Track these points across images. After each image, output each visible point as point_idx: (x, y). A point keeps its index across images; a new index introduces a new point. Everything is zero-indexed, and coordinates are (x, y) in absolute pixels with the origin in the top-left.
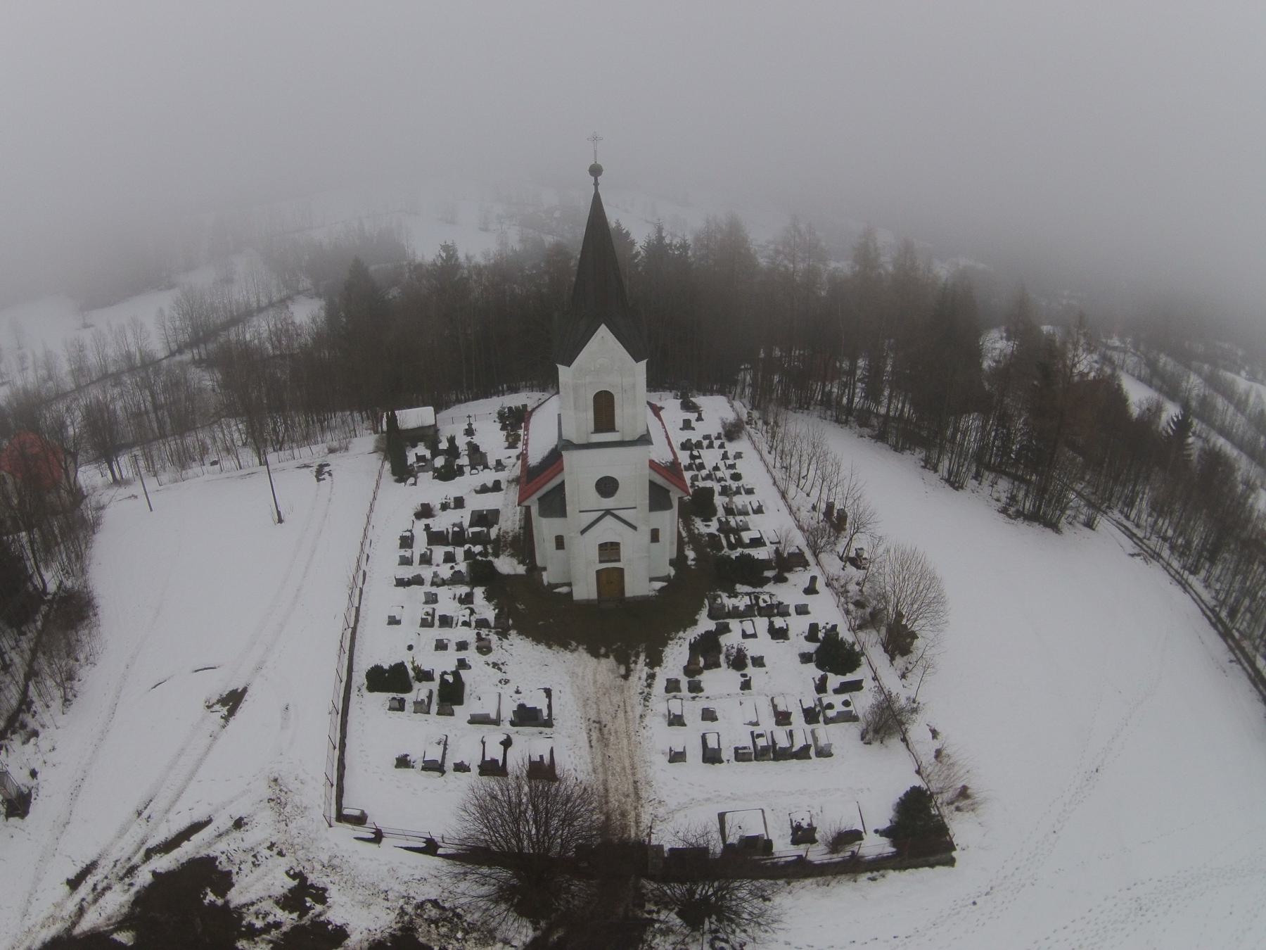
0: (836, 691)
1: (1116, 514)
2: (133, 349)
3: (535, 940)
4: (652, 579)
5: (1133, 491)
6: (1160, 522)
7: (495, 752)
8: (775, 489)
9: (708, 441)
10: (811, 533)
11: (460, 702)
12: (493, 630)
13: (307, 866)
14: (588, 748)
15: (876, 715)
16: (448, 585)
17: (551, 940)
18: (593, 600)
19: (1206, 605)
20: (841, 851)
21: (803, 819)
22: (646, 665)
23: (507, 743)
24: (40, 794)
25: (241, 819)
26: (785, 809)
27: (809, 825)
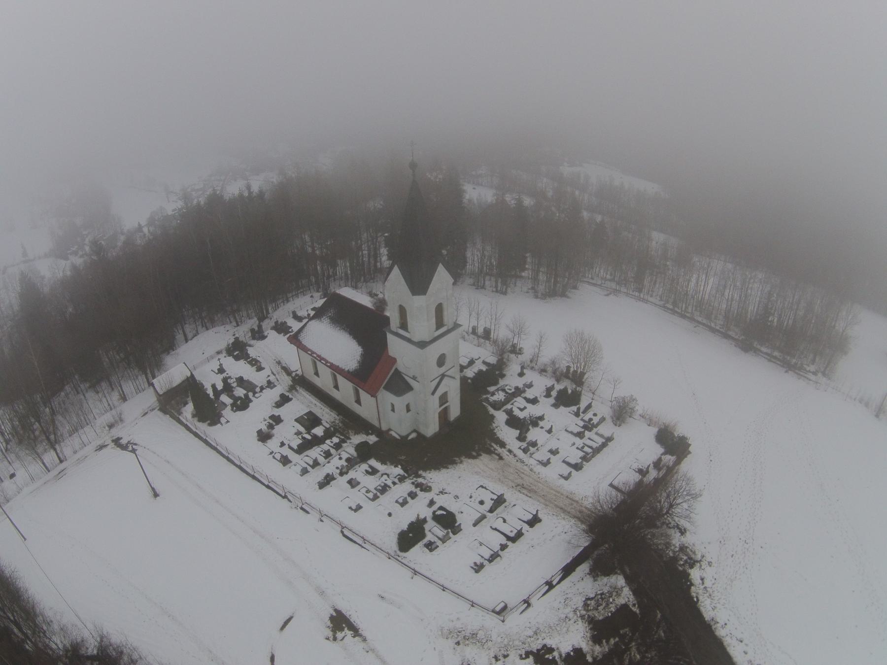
14: (530, 499)
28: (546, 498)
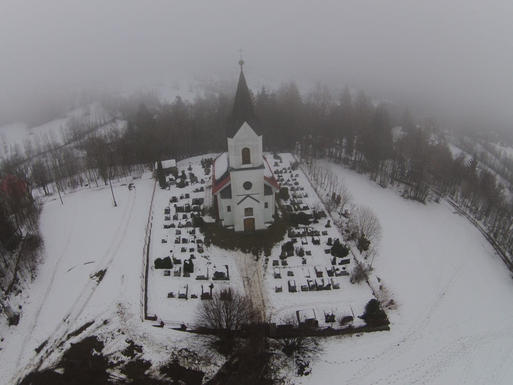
0: (340, 264)
1: (448, 198)
2: (51, 142)
3: (226, 363)
4: (265, 223)
5: (454, 188)
6: (465, 200)
7: (207, 290)
8: (312, 188)
9: (285, 170)
10: (327, 204)
11: (192, 272)
12: (204, 244)
13: (134, 338)
15: (356, 272)
16: (185, 227)
17: (233, 363)
18: (242, 231)
19: (484, 232)
20: (345, 324)
21: (329, 313)
22: (265, 255)
23: (212, 287)
24: (23, 315)
25: (106, 320)
26: (322, 309)
27: (332, 315)
28: (251, 293)
